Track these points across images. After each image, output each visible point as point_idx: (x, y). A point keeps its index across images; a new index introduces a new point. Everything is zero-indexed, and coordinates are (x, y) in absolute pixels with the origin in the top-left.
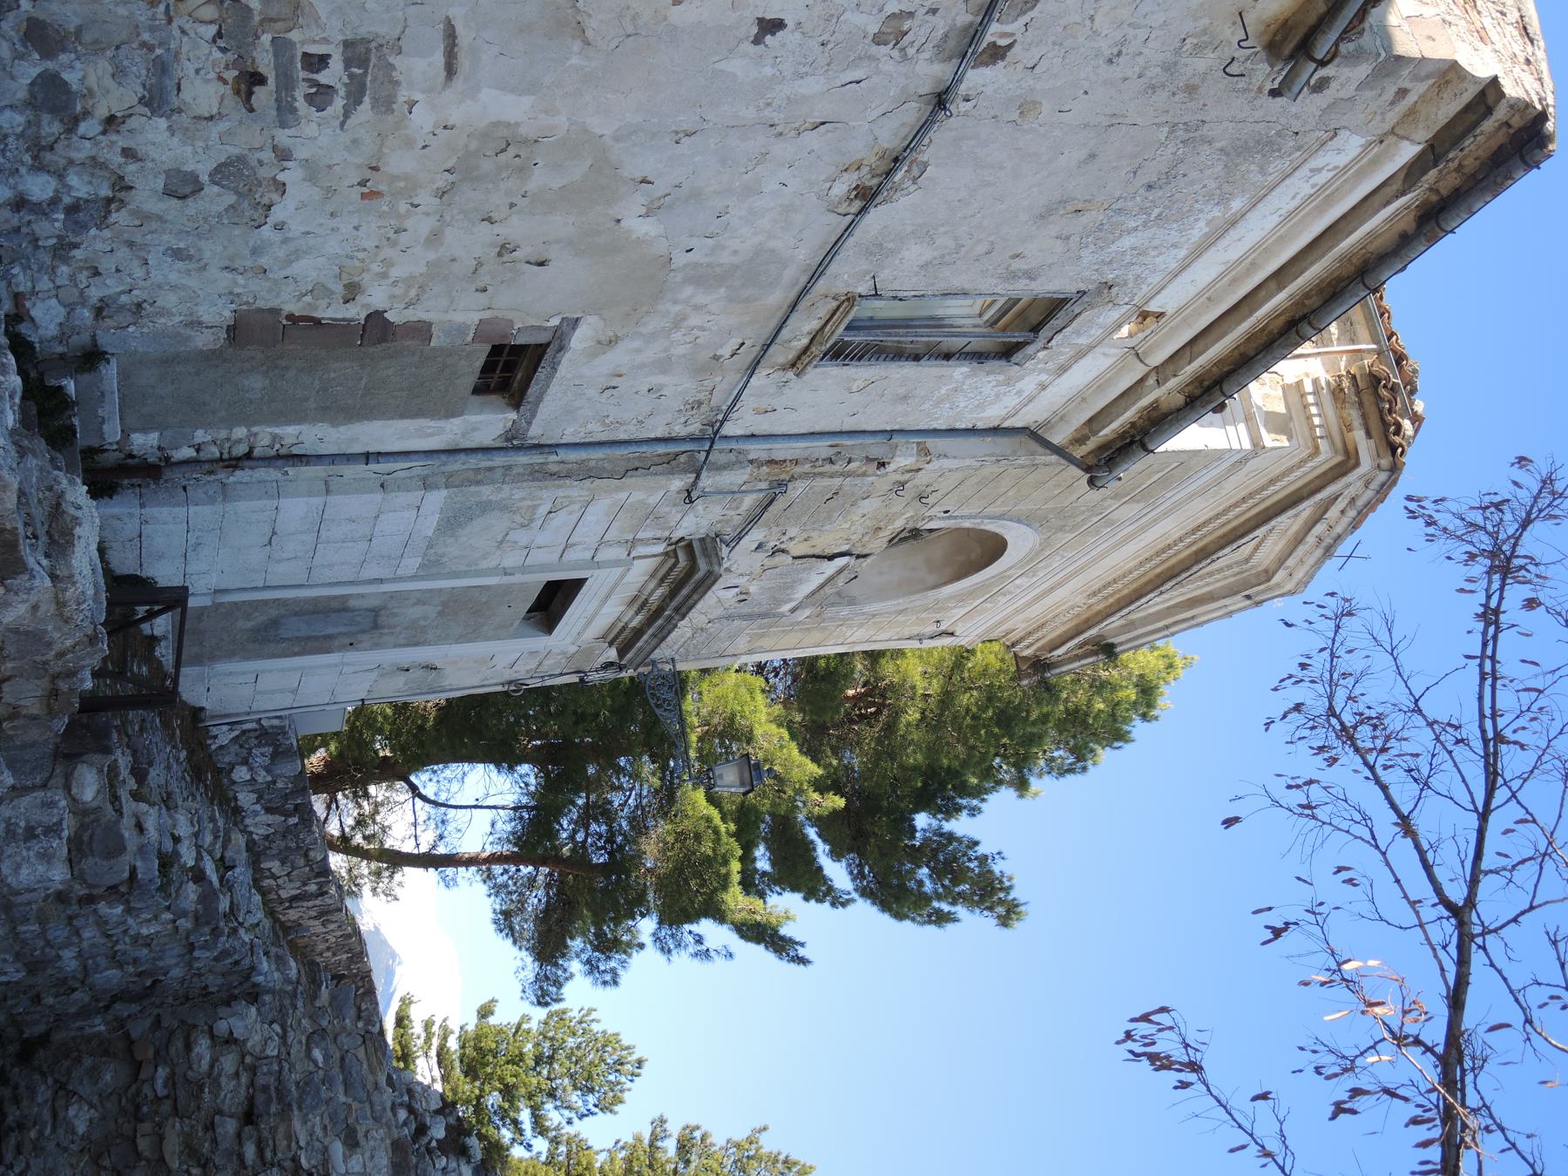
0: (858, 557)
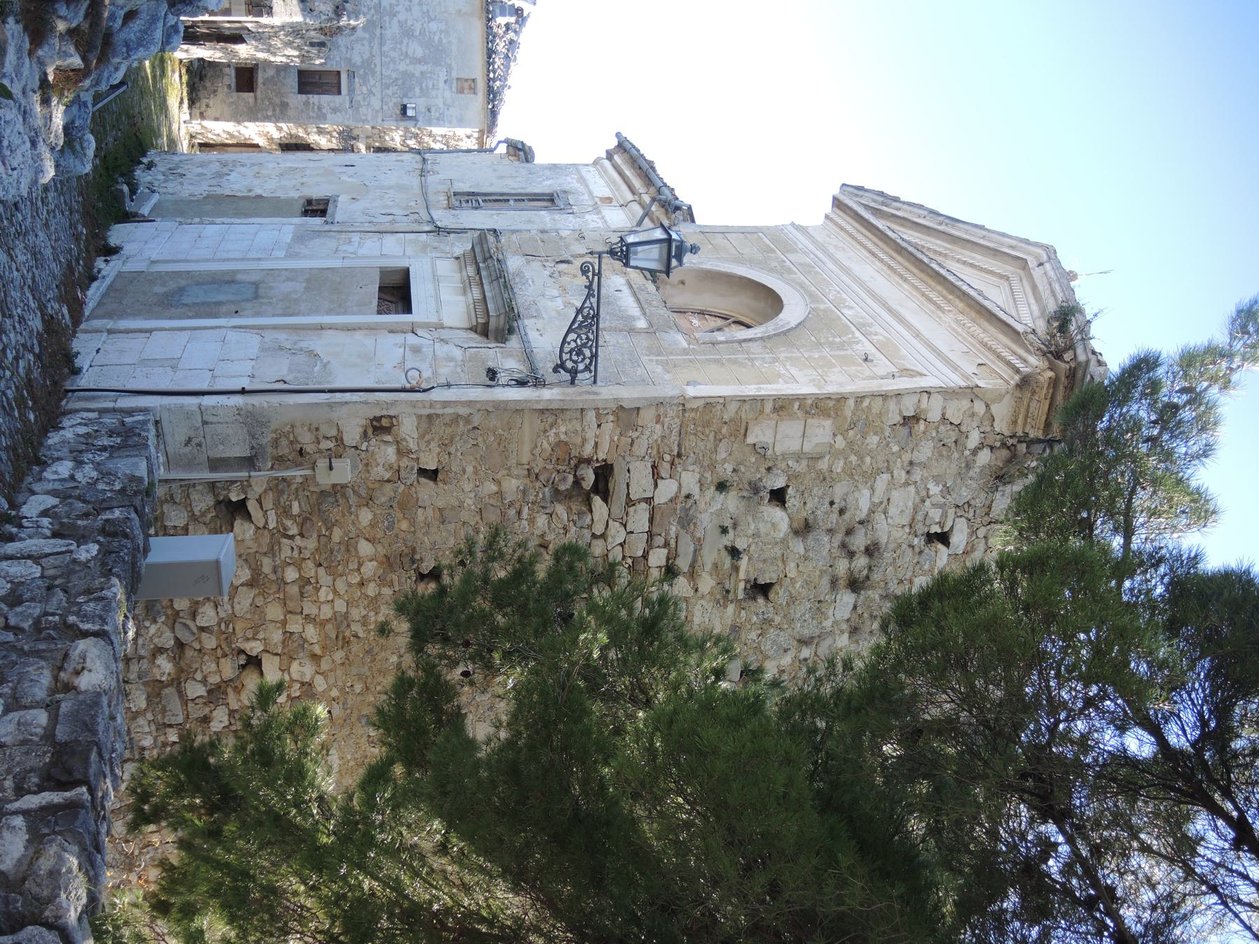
0: (425, 391)
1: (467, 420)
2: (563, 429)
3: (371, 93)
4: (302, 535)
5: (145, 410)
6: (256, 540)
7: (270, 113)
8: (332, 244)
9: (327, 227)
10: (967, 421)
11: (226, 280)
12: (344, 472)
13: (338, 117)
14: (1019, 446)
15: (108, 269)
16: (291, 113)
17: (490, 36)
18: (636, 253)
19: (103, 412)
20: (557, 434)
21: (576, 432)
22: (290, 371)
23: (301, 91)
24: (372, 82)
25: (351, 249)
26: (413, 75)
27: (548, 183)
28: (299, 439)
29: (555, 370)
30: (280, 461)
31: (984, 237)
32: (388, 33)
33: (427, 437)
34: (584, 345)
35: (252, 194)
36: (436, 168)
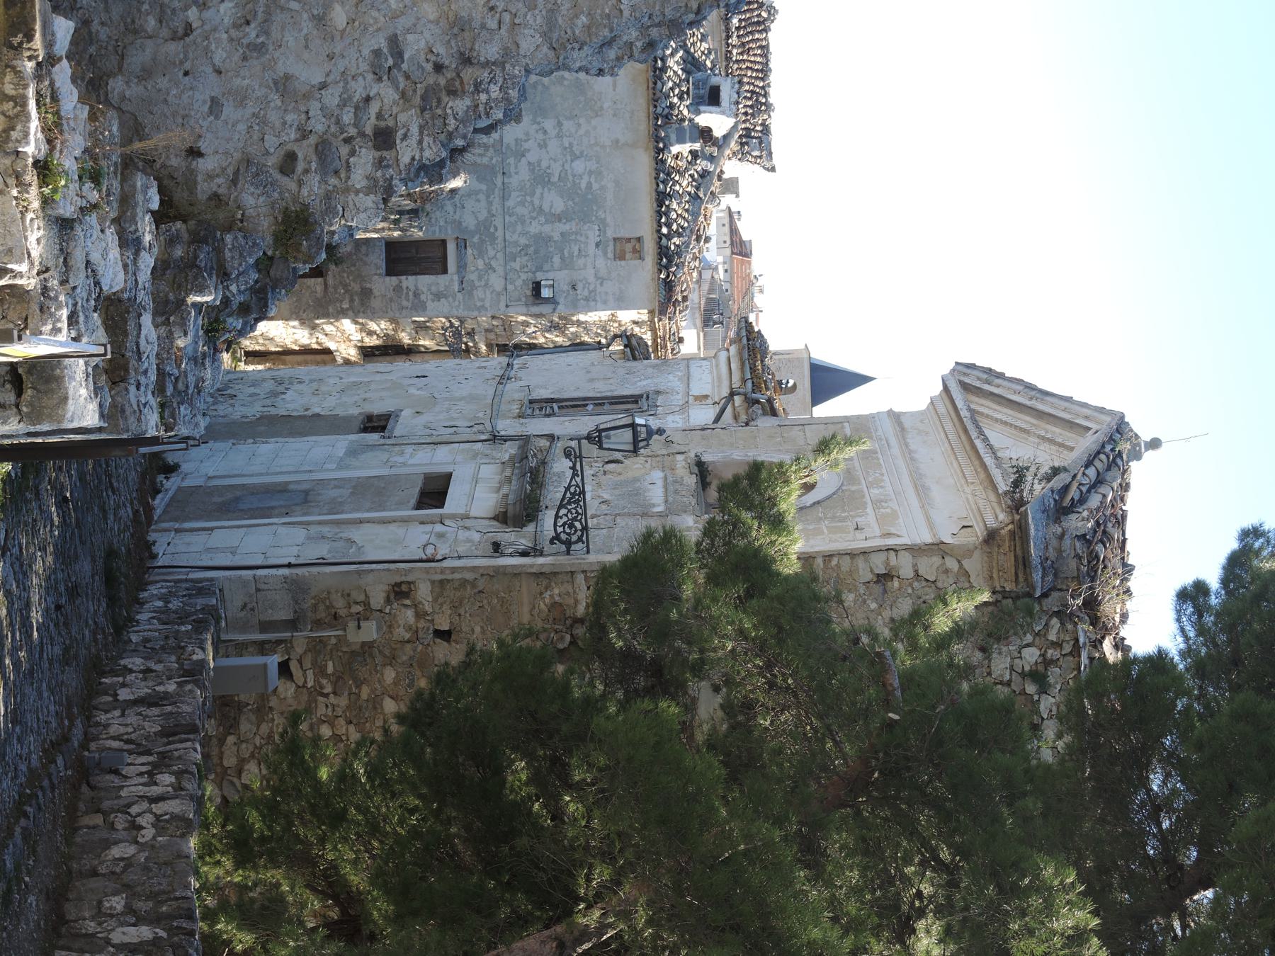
1: (473, 584)
2: (556, 591)
3: (489, 268)
4: (335, 693)
5: (211, 580)
6: (296, 697)
7: (346, 306)
8: (385, 456)
9: (382, 441)
10: (942, 577)
11: (281, 490)
12: (370, 631)
13: (444, 305)
14: (1004, 602)
15: (171, 484)
16: (376, 303)
17: (662, 173)
18: (608, 437)
19: (176, 581)
20: (551, 596)
21: (568, 594)
22: (329, 552)
23: (390, 272)
24: (491, 253)
25: (401, 459)
26: (550, 238)
27: (644, 383)
28: (334, 603)
29: (552, 542)
30: (318, 624)
31: (1065, 410)
32: (514, 181)
33: (440, 600)
34: (575, 519)
35: (309, 413)
36: (520, 374)
